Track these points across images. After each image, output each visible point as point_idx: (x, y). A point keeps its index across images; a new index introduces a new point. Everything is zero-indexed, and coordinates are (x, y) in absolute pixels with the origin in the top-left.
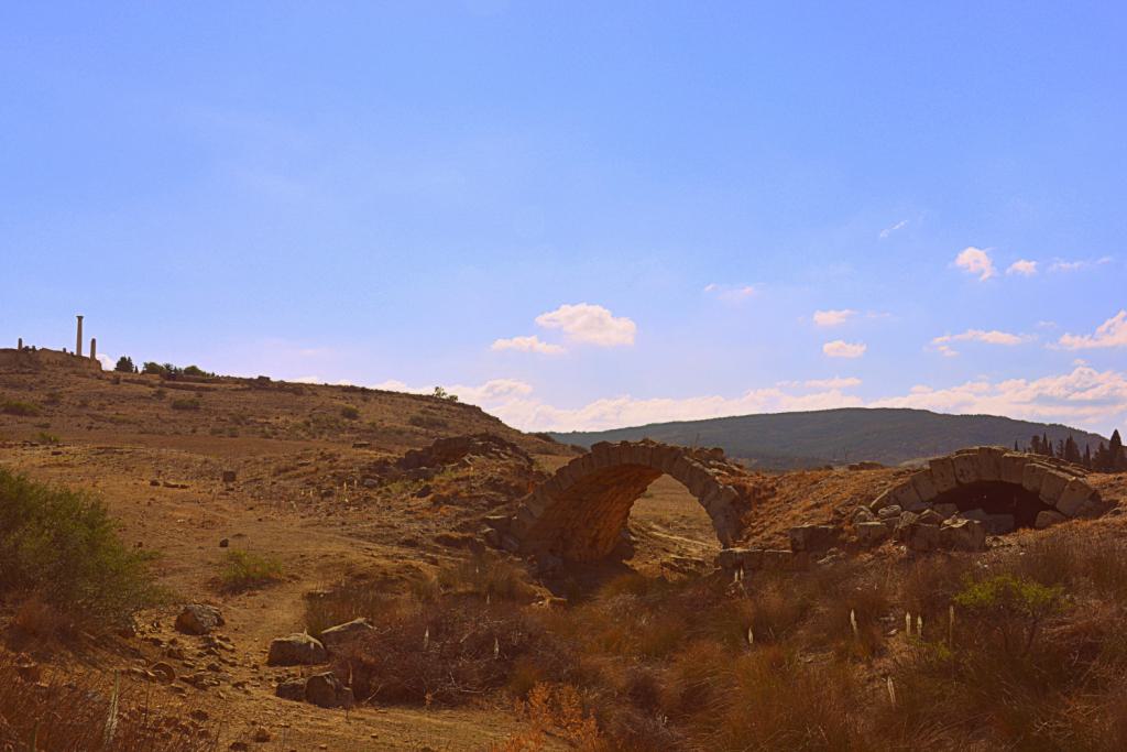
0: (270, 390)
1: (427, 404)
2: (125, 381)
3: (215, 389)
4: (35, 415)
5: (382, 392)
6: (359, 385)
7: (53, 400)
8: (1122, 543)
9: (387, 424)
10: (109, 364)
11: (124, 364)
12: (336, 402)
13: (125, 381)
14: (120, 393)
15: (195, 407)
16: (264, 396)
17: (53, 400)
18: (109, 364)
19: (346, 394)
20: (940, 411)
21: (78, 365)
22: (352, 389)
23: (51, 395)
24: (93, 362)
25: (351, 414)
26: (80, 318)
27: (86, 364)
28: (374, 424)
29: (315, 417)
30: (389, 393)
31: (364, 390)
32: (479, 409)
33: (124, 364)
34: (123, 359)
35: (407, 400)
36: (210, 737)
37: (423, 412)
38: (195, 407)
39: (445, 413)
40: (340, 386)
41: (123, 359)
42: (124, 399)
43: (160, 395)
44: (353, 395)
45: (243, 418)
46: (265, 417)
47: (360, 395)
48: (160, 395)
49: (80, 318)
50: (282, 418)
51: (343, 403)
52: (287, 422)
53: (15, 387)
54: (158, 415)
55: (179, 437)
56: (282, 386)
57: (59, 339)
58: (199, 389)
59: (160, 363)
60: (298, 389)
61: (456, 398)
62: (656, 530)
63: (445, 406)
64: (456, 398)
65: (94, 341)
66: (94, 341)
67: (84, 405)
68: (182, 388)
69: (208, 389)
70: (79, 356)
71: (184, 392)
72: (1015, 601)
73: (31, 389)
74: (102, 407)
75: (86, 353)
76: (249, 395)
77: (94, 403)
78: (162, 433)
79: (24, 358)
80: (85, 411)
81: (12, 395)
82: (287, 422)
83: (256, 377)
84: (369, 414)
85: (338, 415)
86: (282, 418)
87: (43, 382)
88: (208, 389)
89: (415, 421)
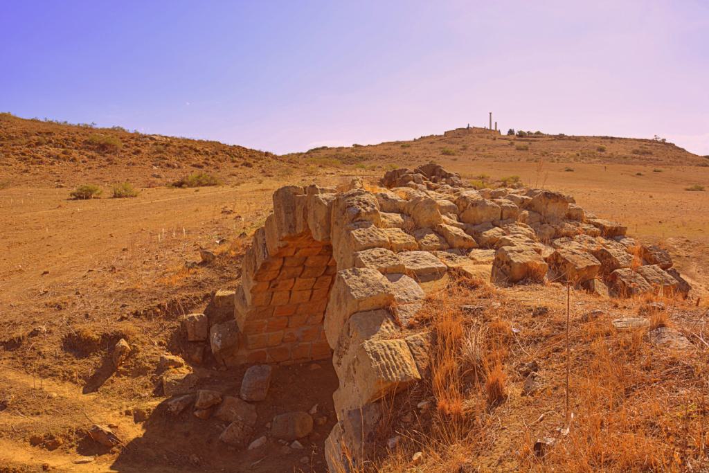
1: (644, 143)
3: (538, 141)
5: (621, 138)
6: (610, 135)
7: (465, 148)
8: (6, 175)
9: (619, 153)
10: (504, 133)
11: (511, 132)
12: (596, 144)
16: (560, 142)
19: (602, 140)
21: (489, 134)
23: (464, 146)
25: (602, 150)
26: (491, 114)
27: (493, 132)
28: (612, 154)
29: (583, 152)
30: (625, 139)
31: (612, 138)
32: (674, 145)
33: (511, 132)
34: (510, 130)
35: (634, 142)
37: (640, 147)
39: (654, 147)
40: (600, 137)
41: (510, 130)
42: (495, 146)
43: (512, 144)
44: (606, 140)
45: (546, 153)
47: (610, 140)
48: (512, 144)
49: (491, 114)
50: (567, 153)
51: (599, 145)
52: (568, 154)
53: (452, 143)
56: (570, 138)
57: (482, 123)
59: (525, 131)
60: (577, 139)
61: (665, 140)
63: (654, 144)
64: (665, 140)
65: (496, 123)
66: (496, 123)
68: (524, 141)
69: (535, 141)
70: (491, 130)
71: (524, 142)
73: (458, 144)
74: (484, 151)
75: (493, 128)
76: (554, 142)
78: (504, 161)
79: (4, 115)
80: (477, 152)
81: (708, 160)
82: (568, 154)
83: (558, 134)
84: (610, 149)
86: (567, 153)
88: (535, 141)
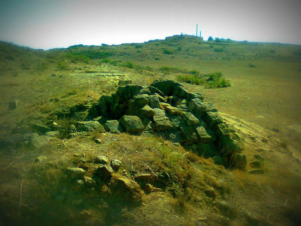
4: (172, 54)
7: (179, 49)
10: (206, 39)
11: (210, 39)
14: (106, 52)
15: (222, 51)
17: (179, 49)
18: (206, 39)
20: (283, 43)
23: (179, 48)
24: (201, 38)
26: (197, 25)
34: (210, 37)
36: (169, 190)
38: (222, 51)
42: (200, 48)
46: (243, 53)
49: (197, 25)
54: (208, 53)
55: (212, 60)
58: (225, 45)
65: (201, 32)
67: (188, 51)
68: (220, 45)
70: (197, 37)
75: (199, 36)
77: (190, 50)
87: (178, 44)
88: (227, 45)
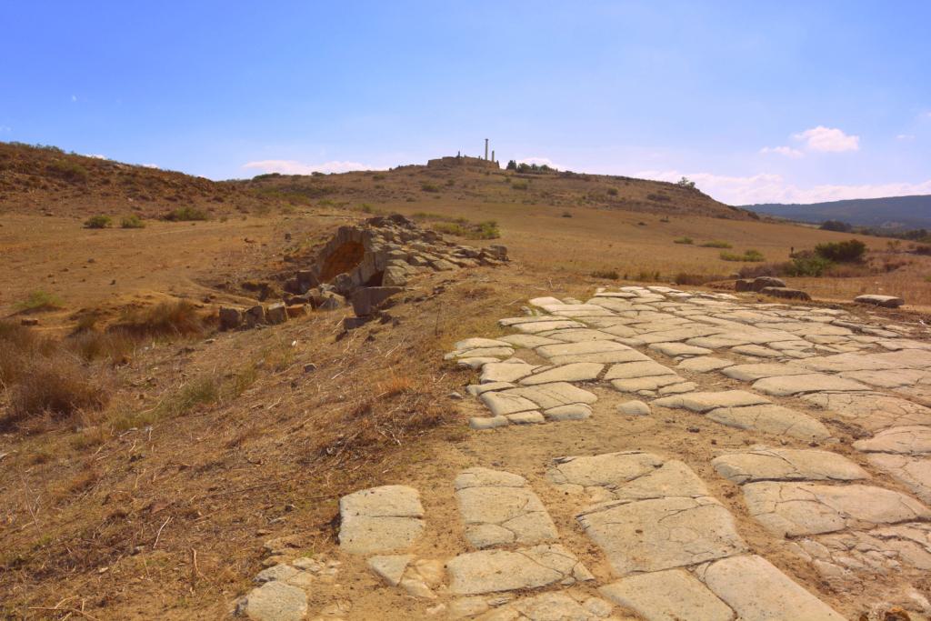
0: (574, 178)
2: (494, 173)
6: (625, 175)
11: (512, 165)
13: (494, 173)
20: (753, 204)
21: (483, 167)
22: (622, 178)
23: (450, 181)
25: (613, 193)
26: (487, 140)
31: (628, 179)
33: (512, 165)
34: (511, 161)
41: (511, 161)
44: (622, 181)
48: (508, 181)
49: (487, 140)
57: (475, 152)
62: (488, 257)
70: (486, 161)
71: (523, 179)
72: (881, 286)
75: (489, 159)
84: (623, 192)
85: (605, 193)
89: (651, 197)
